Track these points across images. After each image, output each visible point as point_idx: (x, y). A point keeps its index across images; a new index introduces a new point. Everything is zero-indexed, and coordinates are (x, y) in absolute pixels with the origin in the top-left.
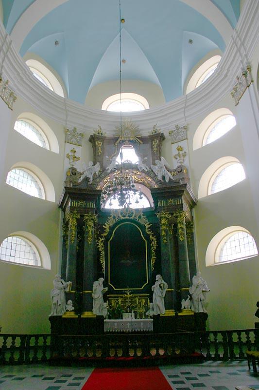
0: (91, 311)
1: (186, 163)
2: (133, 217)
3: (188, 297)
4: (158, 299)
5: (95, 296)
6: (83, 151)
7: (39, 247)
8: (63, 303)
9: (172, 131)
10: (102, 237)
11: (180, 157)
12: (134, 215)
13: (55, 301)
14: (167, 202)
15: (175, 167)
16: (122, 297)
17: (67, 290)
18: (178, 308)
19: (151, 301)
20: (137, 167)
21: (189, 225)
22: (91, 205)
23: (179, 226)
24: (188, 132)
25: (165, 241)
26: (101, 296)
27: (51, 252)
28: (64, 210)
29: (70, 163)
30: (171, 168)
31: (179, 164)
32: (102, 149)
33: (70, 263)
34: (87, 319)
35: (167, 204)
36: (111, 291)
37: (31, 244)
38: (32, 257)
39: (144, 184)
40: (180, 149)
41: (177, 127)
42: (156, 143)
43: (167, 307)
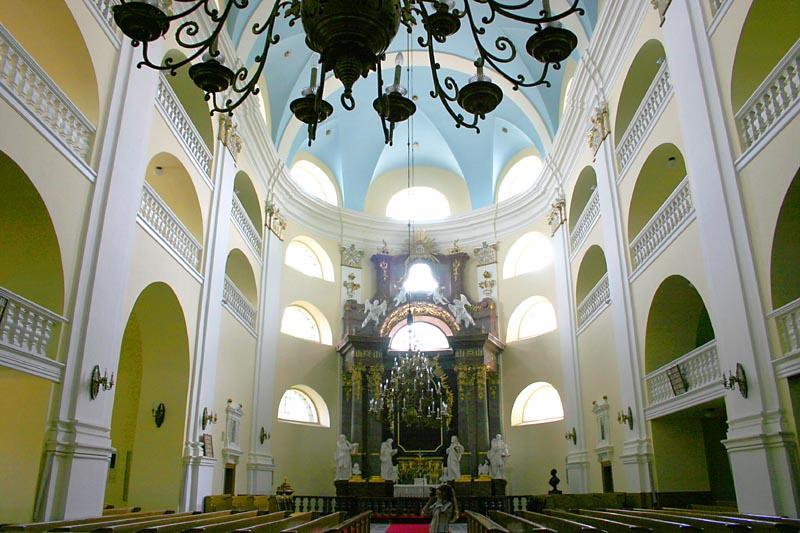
0: (379, 475)
1: (494, 295)
6: (363, 276)
7: (306, 391)
9: (478, 250)
13: (340, 464)
15: (480, 300)
17: (354, 452)
18: (475, 474)
19: (445, 465)
21: (493, 375)
22: (378, 354)
23: (479, 381)
24: (498, 253)
26: (390, 458)
28: (344, 356)
30: (474, 299)
31: (485, 297)
32: (388, 273)
33: (356, 423)
36: (400, 453)
37: (305, 396)
38: (307, 412)
39: (441, 318)
40: (487, 275)
41: (484, 243)
42: (457, 265)
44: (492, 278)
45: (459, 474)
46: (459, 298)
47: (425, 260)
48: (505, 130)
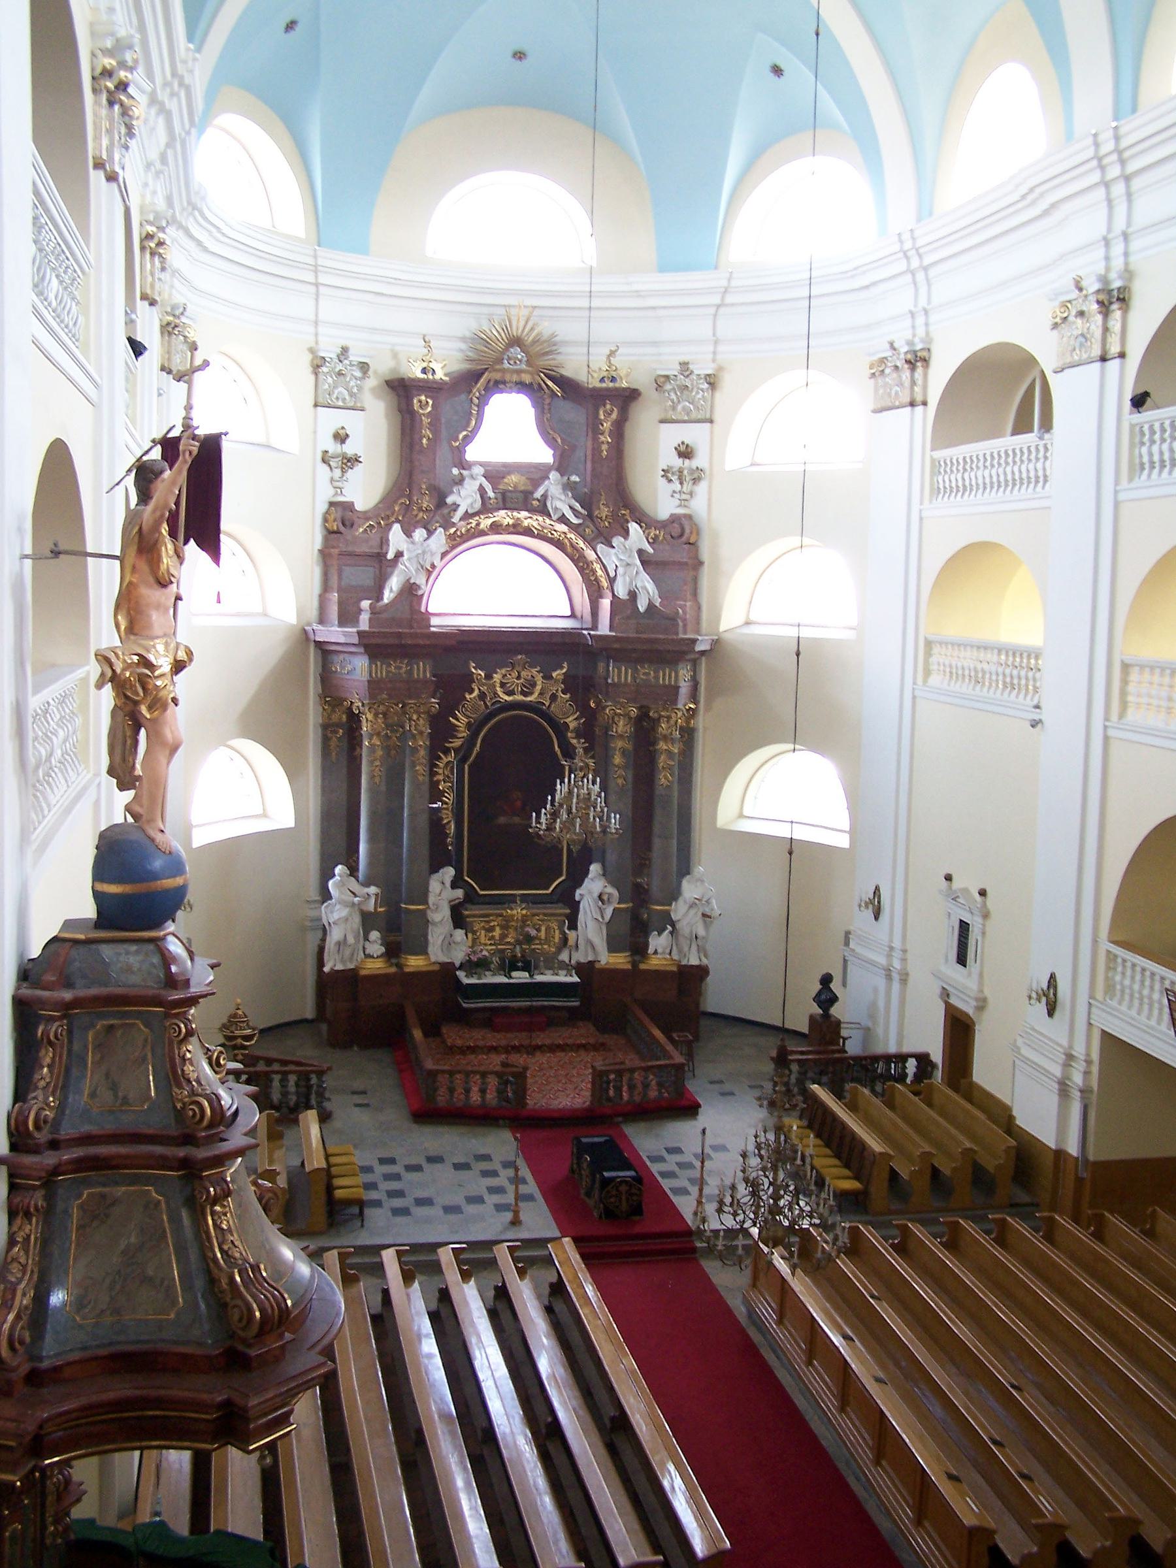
1: (698, 506)
2: (536, 694)
3: (665, 929)
4: (591, 925)
5: (431, 915)
8: (357, 937)
9: (667, 377)
10: (446, 751)
11: (681, 483)
12: (539, 688)
14: (635, 671)
16: (501, 915)
17: (370, 906)
18: (639, 950)
19: (573, 926)
20: (545, 505)
23: (662, 745)
24: (718, 395)
25: (620, 781)
26: (446, 912)
27: (293, 772)
29: (332, 480)
34: (418, 975)
35: (634, 678)
36: (471, 898)
40: (685, 453)
41: (684, 365)
43: (612, 948)
44: (694, 463)
45: (600, 943)
46: (626, 533)
47: (523, 387)
48: (777, 71)
